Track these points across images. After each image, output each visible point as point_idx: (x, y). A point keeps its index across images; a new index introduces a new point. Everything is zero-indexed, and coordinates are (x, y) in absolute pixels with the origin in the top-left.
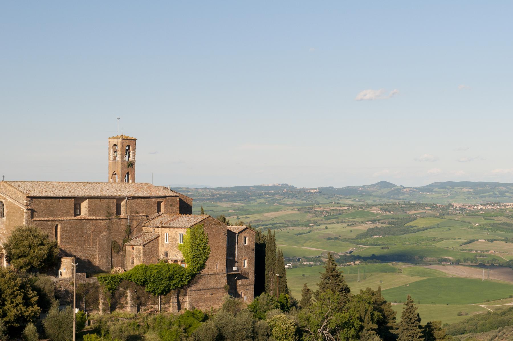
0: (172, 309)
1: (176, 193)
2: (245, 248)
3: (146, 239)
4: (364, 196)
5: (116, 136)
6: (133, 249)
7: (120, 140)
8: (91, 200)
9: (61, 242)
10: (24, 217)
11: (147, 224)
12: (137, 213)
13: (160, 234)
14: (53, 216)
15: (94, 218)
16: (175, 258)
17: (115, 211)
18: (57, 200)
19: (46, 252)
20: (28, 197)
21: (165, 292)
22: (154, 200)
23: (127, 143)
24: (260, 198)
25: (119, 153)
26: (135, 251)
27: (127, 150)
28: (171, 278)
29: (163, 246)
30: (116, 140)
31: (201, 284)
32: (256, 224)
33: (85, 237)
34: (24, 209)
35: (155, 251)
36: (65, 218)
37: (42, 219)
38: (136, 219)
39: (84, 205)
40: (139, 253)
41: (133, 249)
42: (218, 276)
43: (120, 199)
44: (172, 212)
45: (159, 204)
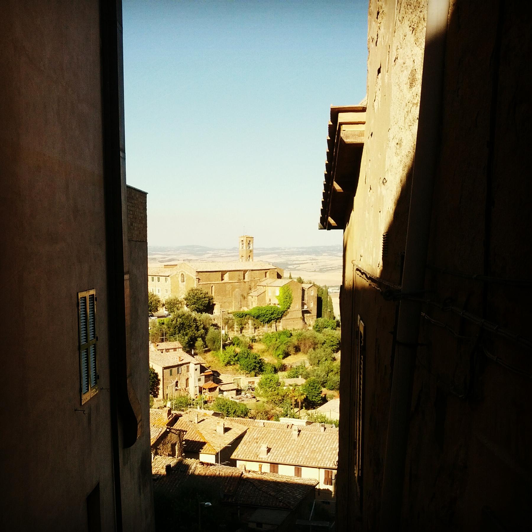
0: (273, 329)
1: (275, 267)
2: (312, 296)
3: (259, 292)
4: (260, 446)
5: (243, 236)
6: (252, 297)
7: (245, 238)
8: (230, 272)
9: (214, 295)
10: (195, 282)
11: (260, 284)
12: (254, 278)
13: (266, 289)
14: (210, 281)
15: (232, 281)
16: (274, 303)
17: (243, 278)
18: (212, 273)
19: (207, 302)
20: (197, 272)
21: (269, 321)
22: (263, 271)
23: (249, 239)
24: (324, 253)
25: (245, 245)
26: (253, 299)
27: (249, 244)
28: (272, 314)
29: (268, 296)
30: (243, 238)
31: (288, 316)
32: (322, 267)
33: (227, 292)
34: (195, 277)
35: (264, 299)
36: (216, 282)
37: (204, 283)
38: (254, 282)
39: (226, 276)
40: (256, 299)
41: (252, 297)
42: (297, 312)
43: (245, 271)
44: (273, 277)
45: (266, 273)
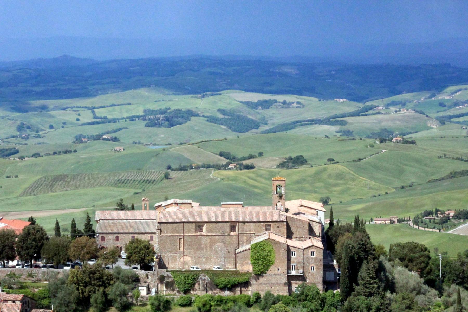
12: (246, 231)
42: (279, 276)
